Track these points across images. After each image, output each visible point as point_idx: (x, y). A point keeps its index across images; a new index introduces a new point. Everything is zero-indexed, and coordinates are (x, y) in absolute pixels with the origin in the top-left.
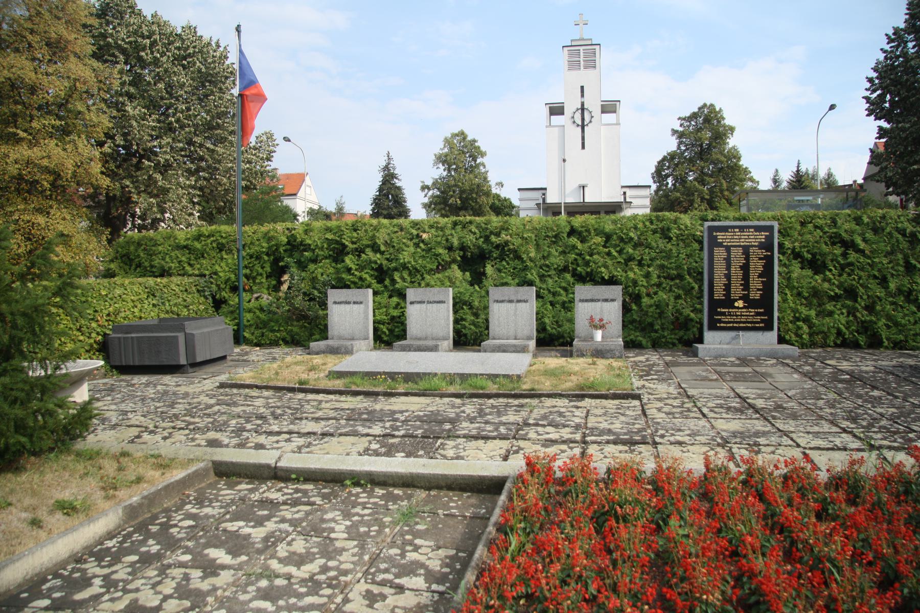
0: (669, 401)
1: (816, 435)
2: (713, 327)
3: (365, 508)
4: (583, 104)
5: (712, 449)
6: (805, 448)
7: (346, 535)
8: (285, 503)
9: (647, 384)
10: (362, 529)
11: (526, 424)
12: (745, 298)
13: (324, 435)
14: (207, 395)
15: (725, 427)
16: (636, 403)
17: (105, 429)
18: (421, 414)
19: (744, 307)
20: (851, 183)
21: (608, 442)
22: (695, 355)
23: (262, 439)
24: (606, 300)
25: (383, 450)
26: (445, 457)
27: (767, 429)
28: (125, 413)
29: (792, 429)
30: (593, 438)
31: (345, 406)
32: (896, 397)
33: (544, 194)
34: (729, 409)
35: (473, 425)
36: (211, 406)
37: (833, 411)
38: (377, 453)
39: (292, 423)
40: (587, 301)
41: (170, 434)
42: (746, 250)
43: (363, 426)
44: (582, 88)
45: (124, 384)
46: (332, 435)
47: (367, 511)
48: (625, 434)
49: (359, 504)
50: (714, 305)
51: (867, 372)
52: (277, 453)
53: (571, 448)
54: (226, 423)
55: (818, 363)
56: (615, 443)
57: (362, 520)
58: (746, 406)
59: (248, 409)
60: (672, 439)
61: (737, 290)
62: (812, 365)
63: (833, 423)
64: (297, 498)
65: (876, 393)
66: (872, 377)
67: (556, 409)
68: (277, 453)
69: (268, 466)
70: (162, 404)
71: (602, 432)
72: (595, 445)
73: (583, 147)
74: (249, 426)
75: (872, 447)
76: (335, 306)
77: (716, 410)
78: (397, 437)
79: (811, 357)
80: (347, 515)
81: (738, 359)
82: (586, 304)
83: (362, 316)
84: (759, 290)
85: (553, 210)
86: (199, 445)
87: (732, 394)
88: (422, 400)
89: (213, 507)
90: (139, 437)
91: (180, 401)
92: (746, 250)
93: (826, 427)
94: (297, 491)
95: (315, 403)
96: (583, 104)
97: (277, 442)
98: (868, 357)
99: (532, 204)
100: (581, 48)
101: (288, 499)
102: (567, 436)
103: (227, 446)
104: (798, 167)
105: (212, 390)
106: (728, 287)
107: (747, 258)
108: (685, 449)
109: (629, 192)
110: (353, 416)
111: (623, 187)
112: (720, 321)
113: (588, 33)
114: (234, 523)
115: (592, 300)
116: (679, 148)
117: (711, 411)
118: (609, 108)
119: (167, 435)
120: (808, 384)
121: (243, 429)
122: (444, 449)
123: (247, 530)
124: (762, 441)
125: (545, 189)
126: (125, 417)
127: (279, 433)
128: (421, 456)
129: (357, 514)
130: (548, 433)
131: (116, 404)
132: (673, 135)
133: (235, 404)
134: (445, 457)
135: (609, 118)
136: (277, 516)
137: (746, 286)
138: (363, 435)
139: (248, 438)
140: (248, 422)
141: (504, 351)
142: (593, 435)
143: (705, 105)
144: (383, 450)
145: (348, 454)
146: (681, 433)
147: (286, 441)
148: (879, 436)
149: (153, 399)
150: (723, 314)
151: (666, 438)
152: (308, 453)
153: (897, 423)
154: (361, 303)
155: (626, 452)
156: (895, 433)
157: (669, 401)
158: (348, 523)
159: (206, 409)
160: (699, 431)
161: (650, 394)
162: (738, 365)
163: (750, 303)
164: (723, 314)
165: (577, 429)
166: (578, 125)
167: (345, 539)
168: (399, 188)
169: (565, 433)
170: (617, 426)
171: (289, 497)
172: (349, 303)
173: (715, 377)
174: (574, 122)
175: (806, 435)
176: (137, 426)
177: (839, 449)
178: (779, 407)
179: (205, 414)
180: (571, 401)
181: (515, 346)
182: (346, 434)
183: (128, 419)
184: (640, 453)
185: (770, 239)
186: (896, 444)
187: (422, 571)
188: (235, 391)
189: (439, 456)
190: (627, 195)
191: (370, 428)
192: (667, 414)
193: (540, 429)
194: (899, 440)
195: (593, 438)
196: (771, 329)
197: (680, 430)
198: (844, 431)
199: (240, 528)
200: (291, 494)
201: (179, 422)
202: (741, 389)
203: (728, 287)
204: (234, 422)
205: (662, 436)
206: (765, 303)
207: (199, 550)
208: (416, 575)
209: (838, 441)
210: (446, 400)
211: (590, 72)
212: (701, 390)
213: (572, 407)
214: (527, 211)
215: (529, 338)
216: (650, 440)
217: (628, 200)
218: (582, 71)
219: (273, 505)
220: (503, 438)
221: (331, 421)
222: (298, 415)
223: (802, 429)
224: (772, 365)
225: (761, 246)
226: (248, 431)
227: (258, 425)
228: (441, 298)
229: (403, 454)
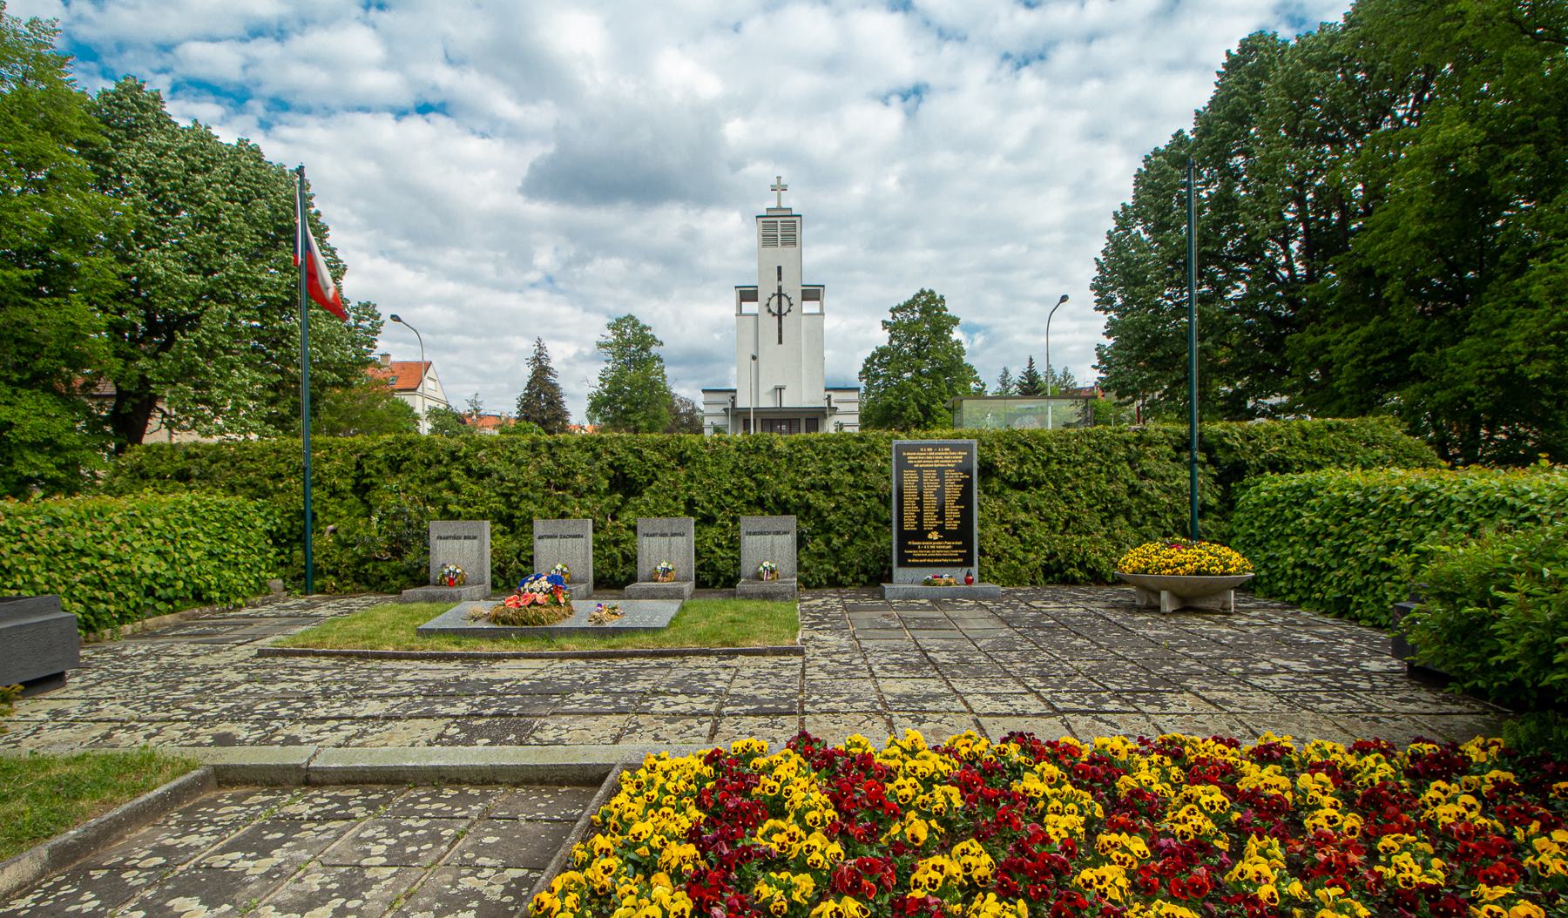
0: (836, 657)
1: (996, 697)
2: (903, 563)
3: (423, 818)
4: (780, 288)
5: (869, 719)
6: (978, 714)
7: (384, 860)
8: (311, 819)
9: (817, 635)
10: (409, 850)
11: (655, 693)
12: (940, 529)
13: (388, 718)
14: (236, 669)
15: (892, 690)
16: (798, 659)
17: (54, 728)
18: (527, 683)
19: (939, 540)
21: (747, 714)
22: (882, 597)
23: (298, 730)
24: (778, 533)
25: (463, 735)
26: (541, 743)
27: (941, 690)
28: (95, 701)
29: (970, 690)
30: (731, 709)
31: (429, 676)
32: (1100, 647)
33: (733, 397)
34: (904, 665)
35: (589, 697)
36: (238, 684)
37: (1023, 665)
38: (454, 742)
39: (348, 704)
40: (755, 534)
41: (159, 729)
42: (941, 472)
43: (444, 703)
44: (779, 268)
45: (108, 656)
46: (398, 718)
47: (423, 823)
48: (771, 701)
49: (415, 812)
50: (904, 537)
51: (1074, 616)
52: (312, 748)
53: (701, 723)
54: (250, 709)
55: (1023, 605)
56: (755, 714)
57: (414, 835)
58: (925, 663)
59: (289, 686)
60: (824, 707)
61: (930, 521)
62: (1015, 607)
63: (1019, 681)
64: (329, 811)
65: (1079, 642)
66: (1079, 621)
67: (699, 671)
68: (312, 748)
69: (297, 767)
70: (160, 685)
71: (747, 700)
72: (731, 718)
73: (780, 342)
74: (283, 712)
75: (1057, 712)
76: (439, 542)
77: (889, 667)
78: (487, 716)
79: (1015, 597)
80: (393, 830)
81: (931, 601)
82: (754, 538)
83: (476, 554)
84: (955, 519)
85: (740, 416)
86: (200, 744)
87: (913, 646)
88: (537, 663)
89: (201, 834)
90: (107, 736)
91: (192, 679)
92: (941, 472)
93: (1012, 686)
94: (333, 799)
95: (390, 674)
96: (780, 288)
97: (318, 732)
98: (1081, 595)
99: (719, 409)
100: (779, 220)
101: (317, 813)
102: (699, 707)
103: (242, 743)
104: (1030, 367)
105: (246, 661)
106: (920, 517)
107: (942, 483)
108: (837, 720)
109: (835, 396)
110: (438, 691)
112: (911, 556)
113: (790, 201)
114: (226, 856)
115: (761, 533)
116: (890, 343)
117: (883, 668)
118: (812, 293)
119: (154, 731)
120: (1005, 632)
121: (274, 716)
122: (541, 731)
123: (242, 864)
124: (930, 706)
125: (735, 391)
126: (94, 707)
127: (323, 720)
128: (510, 743)
129: (409, 828)
130: (677, 704)
131: (84, 688)
132: (885, 328)
133: (273, 680)
134: (541, 743)
135: (810, 307)
136: (293, 840)
137: (941, 515)
138: (441, 717)
139: (277, 728)
140: (283, 705)
141: (654, 597)
142: (732, 705)
143: (923, 292)
144: (463, 735)
145: (413, 745)
146: (838, 699)
147: (331, 731)
148: (1068, 696)
149: (148, 679)
150: (915, 548)
151: (818, 706)
152: (358, 746)
153: (1092, 679)
154: (475, 538)
155: (767, 725)
156: (1087, 692)
157: (836, 657)
158: (392, 841)
159: (226, 688)
160: (859, 695)
161: (817, 647)
162: (929, 609)
163: (947, 535)
164: (915, 548)
165: (715, 698)
167: (381, 866)
168: (554, 386)
169: (699, 703)
170: (764, 693)
171: (320, 809)
172: (458, 538)
173: (897, 625)
174: (770, 311)
175: (983, 698)
176: (110, 721)
177: (1018, 715)
178: (963, 662)
179: (222, 697)
180: (720, 659)
181: (666, 590)
182: (417, 717)
183: (101, 710)
185: (968, 458)
186: (1082, 707)
187: (475, 904)
188: (280, 660)
189: (533, 742)
190: (833, 399)
191: (454, 705)
192: (829, 673)
193: (670, 699)
194: (1089, 702)
195: (731, 709)
196: (972, 565)
197: (838, 694)
198: (1030, 691)
199: (233, 862)
200: (323, 805)
201: (178, 711)
202: (926, 639)
203: (920, 517)
204: (263, 706)
205: (814, 703)
206: (963, 534)
207: (159, 901)
208: (465, 910)
209: (1018, 705)
210: (568, 663)
211: (789, 250)
212: (877, 642)
213: (720, 666)
214: (712, 416)
215: (686, 579)
216: (796, 710)
217: (833, 405)
218: (780, 249)
219: (294, 823)
220: (621, 712)
221: (403, 699)
222: (360, 693)
223: (982, 690)
224: (969, 608)
225: (958, 468)
226: (282, 718)
227: (299, 710)
228: (578, 532)
229: (487, 741)
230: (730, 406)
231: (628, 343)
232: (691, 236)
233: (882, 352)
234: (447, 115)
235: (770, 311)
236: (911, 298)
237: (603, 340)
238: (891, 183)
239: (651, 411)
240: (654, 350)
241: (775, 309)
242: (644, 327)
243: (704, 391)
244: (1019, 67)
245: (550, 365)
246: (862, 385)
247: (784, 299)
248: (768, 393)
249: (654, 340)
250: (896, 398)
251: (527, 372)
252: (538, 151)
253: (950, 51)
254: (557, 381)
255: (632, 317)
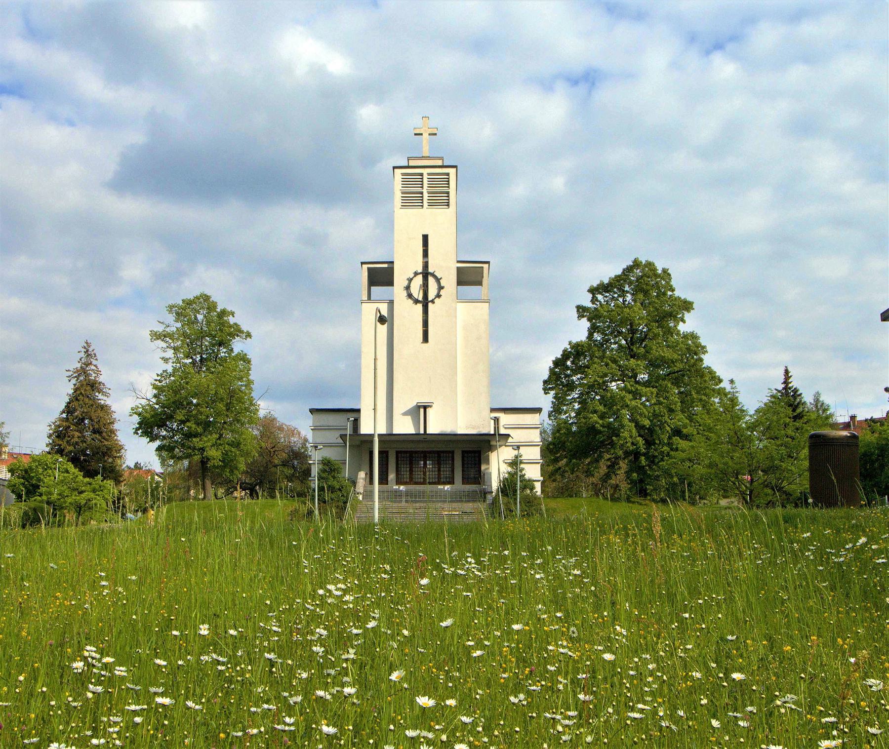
4: (426, 265)
20: (847, 419)
44: (425, 238)
73: (426, 339)
96: (426, 265)
100: (425, 171)
104: (786, 382)
109: (506, 419)
111: (493, 410)
116: (590, 336)
132: (580, 316)
143: (636, 264)
166: (416, 301)
168: (104, 408)
174: (410, 296)
184: (96, 504)
190: (502, 422)
218: (427, 212)
230: (349, 432)
231: (201, 335)
232: (313, 240)
233: (576, 351)
234: (22, 96)
235: (410, 296)
236: (619, 272)
237: (160, 329)
238: (558, 183)
239: (229, 436)
240: (238, 345)
241: (417, 293)
242: (224, 313)
243: (312, 411)
244: (708, 53)
245: (101, 379)
246: (546, 402)
247: (431, 280)
248: (405, 414)
249: (237, 331)
250: (602, 417)
251: (67, 389)
252: (137, 138)
253: (625, 32)
254: (109, 402)
255: (206, 298)
